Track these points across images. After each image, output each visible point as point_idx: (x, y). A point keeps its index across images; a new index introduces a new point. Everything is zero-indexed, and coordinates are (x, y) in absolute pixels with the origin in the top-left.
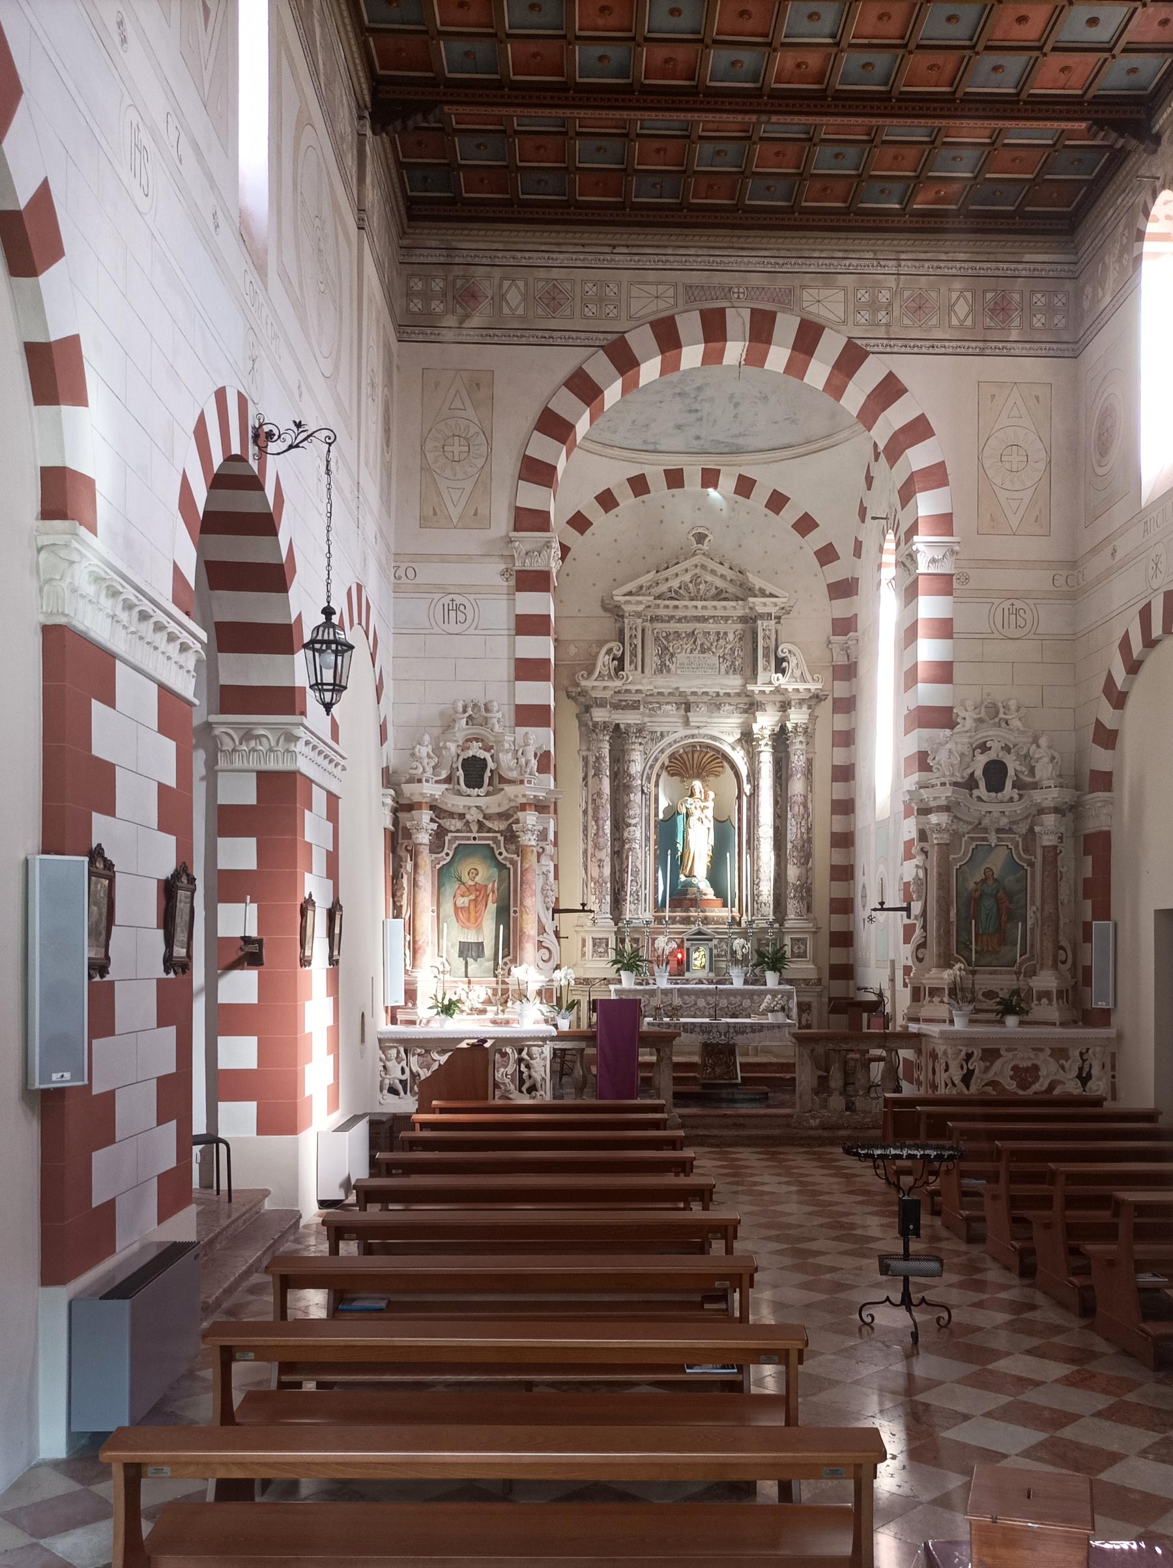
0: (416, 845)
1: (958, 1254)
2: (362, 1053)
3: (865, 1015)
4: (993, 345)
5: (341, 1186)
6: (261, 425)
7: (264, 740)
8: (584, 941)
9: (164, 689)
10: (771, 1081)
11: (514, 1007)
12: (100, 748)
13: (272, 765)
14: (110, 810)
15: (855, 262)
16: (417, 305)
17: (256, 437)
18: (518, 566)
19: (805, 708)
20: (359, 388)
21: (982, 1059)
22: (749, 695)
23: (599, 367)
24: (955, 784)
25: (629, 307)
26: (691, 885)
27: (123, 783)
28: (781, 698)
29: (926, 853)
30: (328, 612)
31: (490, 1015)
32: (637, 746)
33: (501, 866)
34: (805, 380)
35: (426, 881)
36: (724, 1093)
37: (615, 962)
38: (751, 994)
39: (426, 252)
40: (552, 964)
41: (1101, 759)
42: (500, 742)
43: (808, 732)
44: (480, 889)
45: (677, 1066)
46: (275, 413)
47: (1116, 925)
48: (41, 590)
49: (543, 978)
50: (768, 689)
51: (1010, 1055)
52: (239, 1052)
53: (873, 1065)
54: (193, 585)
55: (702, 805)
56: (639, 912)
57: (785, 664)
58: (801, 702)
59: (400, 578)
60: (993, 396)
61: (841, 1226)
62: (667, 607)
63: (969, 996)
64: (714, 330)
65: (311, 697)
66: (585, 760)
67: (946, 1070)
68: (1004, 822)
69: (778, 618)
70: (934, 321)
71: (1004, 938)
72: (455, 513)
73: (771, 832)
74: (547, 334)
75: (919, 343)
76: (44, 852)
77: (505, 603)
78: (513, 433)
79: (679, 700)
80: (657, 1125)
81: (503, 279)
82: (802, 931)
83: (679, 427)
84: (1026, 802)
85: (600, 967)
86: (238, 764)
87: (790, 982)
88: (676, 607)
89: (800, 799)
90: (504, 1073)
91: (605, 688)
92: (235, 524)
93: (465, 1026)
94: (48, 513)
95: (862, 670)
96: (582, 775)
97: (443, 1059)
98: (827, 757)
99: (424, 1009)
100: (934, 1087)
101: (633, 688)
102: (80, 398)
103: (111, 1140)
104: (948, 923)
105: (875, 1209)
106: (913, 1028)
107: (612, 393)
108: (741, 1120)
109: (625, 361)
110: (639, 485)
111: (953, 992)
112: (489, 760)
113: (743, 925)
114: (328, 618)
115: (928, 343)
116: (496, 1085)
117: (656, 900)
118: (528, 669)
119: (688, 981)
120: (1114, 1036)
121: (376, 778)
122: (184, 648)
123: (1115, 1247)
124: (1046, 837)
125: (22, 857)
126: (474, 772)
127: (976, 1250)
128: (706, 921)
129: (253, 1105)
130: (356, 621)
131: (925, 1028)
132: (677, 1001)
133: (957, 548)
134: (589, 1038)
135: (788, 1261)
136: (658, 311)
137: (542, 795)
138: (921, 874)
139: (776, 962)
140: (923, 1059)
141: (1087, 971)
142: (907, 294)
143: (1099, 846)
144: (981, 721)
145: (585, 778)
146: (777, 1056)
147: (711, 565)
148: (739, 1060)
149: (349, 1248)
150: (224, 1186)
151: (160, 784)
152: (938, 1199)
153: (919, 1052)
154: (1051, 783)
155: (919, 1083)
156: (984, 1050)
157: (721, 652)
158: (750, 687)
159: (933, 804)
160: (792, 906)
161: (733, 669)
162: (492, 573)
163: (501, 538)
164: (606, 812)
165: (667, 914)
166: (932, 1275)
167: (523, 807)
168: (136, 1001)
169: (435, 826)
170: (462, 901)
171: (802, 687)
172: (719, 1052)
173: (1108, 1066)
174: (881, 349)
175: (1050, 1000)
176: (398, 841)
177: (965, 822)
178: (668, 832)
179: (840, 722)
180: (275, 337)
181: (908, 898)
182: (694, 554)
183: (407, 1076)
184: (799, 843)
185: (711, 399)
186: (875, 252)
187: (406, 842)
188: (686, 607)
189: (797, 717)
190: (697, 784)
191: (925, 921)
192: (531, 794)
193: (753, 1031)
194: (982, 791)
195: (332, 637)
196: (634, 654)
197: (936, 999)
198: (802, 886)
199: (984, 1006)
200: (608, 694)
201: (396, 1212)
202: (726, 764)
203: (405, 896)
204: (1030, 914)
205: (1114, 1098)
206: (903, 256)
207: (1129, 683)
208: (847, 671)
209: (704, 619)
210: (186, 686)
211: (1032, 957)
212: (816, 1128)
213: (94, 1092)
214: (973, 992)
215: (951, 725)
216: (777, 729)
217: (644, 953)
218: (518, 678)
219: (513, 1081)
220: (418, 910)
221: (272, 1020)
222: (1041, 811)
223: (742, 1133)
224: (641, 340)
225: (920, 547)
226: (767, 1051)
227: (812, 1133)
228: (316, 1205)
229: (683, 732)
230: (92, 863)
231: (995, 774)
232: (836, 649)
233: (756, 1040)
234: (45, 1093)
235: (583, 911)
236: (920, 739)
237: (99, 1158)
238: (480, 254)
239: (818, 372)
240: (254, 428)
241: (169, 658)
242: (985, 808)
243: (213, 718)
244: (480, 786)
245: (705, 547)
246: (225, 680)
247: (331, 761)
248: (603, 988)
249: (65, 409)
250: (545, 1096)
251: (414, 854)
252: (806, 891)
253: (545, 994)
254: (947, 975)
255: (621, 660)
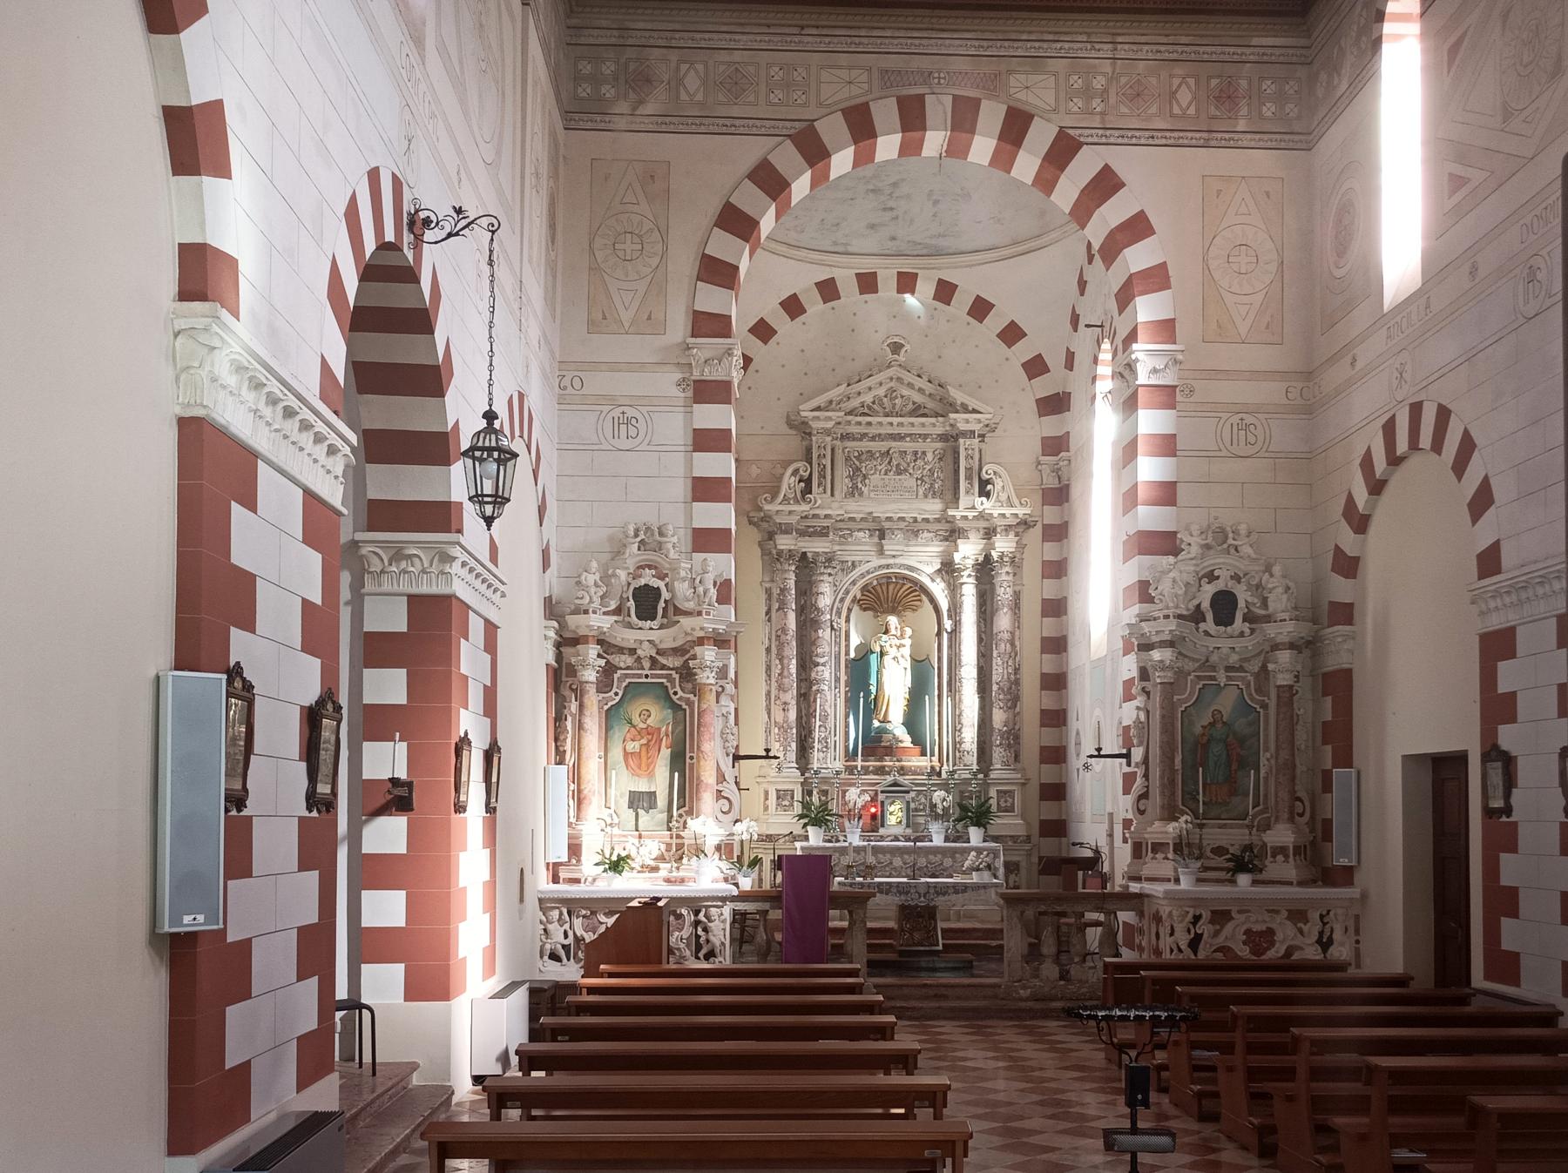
0: (582, 683)
1: (1187, 1132)
2: (521, 912)
3: (1080, 873)
4: (1219, 135)
5: (498, 1060)
6: (417, 211)
7: (416, 561)
8: (766, 793)
9: (309, 494)
10: (975, 948)
11: (690, 865)
12: (241, 556)
13: (424, 589)
14: (249, 626)
15: (1066, 45)
16: (585, 90)
17: (412, 224)
18: (696, 375)
19: (1011, 535)
20: (523, 177)
21: (1212, 922)
22: (950, 521)
23: (786, 157)
24: (1180, 617)
25: (818, 91)
26: (885, 731)
27: (263, 593)
28: (985, 524)
29: (1148, 694)
30: (490, 416)
31: (663, 873)
32: (825, 578)
33: (676, 708)
34: (1013, 173)
35: (593, 723)
36: (924, 962)
37: (801, 817)
38: (954, 851)
39: (595, 32)
40: (732, 817)
41: (1341, 589)
42: (675, 570)
43: (1015, 562)
44: (651, 732)
45: (872, 932)
46: (433, 198)
47: (1359, 773)
48: (177, 379)
49: (722, 831)
50: (970, 514)
51: (1242, 917)
52: (386, 909)
53: (1090, 931)
54: (368, 256)
55: (898, 642)
56: (828, 761)
57: (989, 487)
58: (1008, 528)
59: (565, 388)
60: (1219, 192)
61: (1058, 1103)
62: (859, 423)
63: (1197, 852)
64: (913, 119)
65: (470, 510)
66: (769, 592)
67: (1172, 934)
68: (1234, 658)
69: (982, 436)
70: (1154, 110)
71: (1233, 787)
72: (626, 316)
73: (974, 673)
74: (728, 122)
75: (1137, 134)
76: (177, 668)
77: (681, 416)
78: (691, 232)
79: (872, 526)
80: (851, 989)
81: (680, 61)
82: (1009, 782)
83: (872, 226)
84: (1257, 637)
85: (784, 822)
86: (386, 587)
87: (996, 839)
88: (869, 424)
89: (1006, 636)
90: (679, 937)
91: (790, 512)
92: (387, 317)
93: (635, 885)
94: (185, 295)
95: (1075, 492)
96: (765, 609)
97: (611, 921)
98: (1036, 590)
99: (588, 866)
100: (1158, 952)
101: (822, 512)
102: (223, 170)
103: (246, 994)
104: (1173, 771)
105: (1095, 1085)
106: (1135, 887)
107: (801, 187)
108: (943, 991)
109: (815, 153)
110: (828, 290)
111: (1178, 848)
112: (663, 589)
113: (944, 775)
114: (490, 424)
115: (1147, 134)
116: (670, 951)
117: (847, 747)
118: (706, 490)
119: (882, 838)
120: (1358, 896)
121: (538, 609)
122: (332, 451)
123: (1366, 1120)
124: (1280, 676)
125: (153, 674)
126: (647, 602)
127: (1208, 1130)
128: (902, 771)
129: (402, 966)
130: (517, 433)
131: (1147, 887)
132: (871, 860)
133: (1180, 357)
134: (773, 898)
135: (997, 1141)
136: (851, 98)
137: (721, 627)
138: (1142, 717)
139: (980, 817)
140: (1145, 922)
141: (1327, 823)
142: (1123, 80)
143: (1339, 685)
144: (1208, 547)
145: (768, 613)
146: (982, 922)
147: (908, 378)
148: (941, 925)
149: (513, 1114)
150: (367, 1058)
151: (304, 600)
152: (1165, 1074)
153: (1141, 914)
154: (1286, 616)
155: (1141, 949)
156: (1213, 912)
157: (918, 474)
158: (951, 512)
159: (1155, 639)
160: (998, 755)
161: (931, 493)
162: (667, 383)
163: (678, 345)
164: (792, 650)
165: (859, 763)
166: (1164, 1151)
167: (701, 641)
168: (277, 841)
169: (602, 662)
170: (633, 746)
171: (1008, 511)
172: (918, 916)
173: (1351, 930)
174: (1096, 140)
175: (1286, 856)
176: (561, 678)
177: (1194, 660)
178: (859, 672)
179: (1051, 551)
180: (433, 116)
181: (1128, 744)
182: (889, 366)
183: (571, 940)
184: (1005, 685)
185: (908, 197)
186: (1089, 34)
187: (570, 680)
188: (880, 424)
189: (1003, 545)
190: (893, 620)
191: (1147, 769)
192: (710, 626)
193: (956, 892)
194: (1209, 625)
195: (493, 444)
196: (822, 476)
197: (1160, 856)
198: (1009, 732)
199: (1212, 864)
200: (794, 519)
201: (564, 1080)
202: (924, 598)
203: (569, 741)
204: (1263, 761)
205: (1358, 966)
206: (1120, 39)
207: (1372, 505)
208: (1059, 495)
209: (899, 437)
210: (334, 493)
211: (1265, 810)
212: (1027, 1000)
213: (230, 939)
214: (1200, 847)
215: (1175, 551)
216: (981, 559)
217: (833, 807)
218: (695, 499)
219: (688, 945)
220: (584, 755)
221: (425, 872)
222: (1276, 647)
223: (944, 1004)
224: (832, 128)
225: (1140, 355)
226: (970, 916)
227: (1023, 1005)
228: (469, 1081)
229: (877, 562)
230: (230, 682)
231: (1224, 606)
232: (1046, 470)
233: (958, 902)
234: (175, 937)
235: (767, 757)
236: (1140, 567)
237: (234, 1014)
238: (655, 34)
239: (1027, 165)
240: (409, 214)
241: (315, 461)
242: (1212, 643)
243: (360, 536)
244: (653, 619)
245: (901, 358)
246: (373, 494)
247: (489, 586)
248: (788, 845)
249: (206, 180)
250: (725, 960)
251: (579, 693)
252: (1013, 738)
253: (724, 849)
254: (1172, 828)
255: (808, 481)
